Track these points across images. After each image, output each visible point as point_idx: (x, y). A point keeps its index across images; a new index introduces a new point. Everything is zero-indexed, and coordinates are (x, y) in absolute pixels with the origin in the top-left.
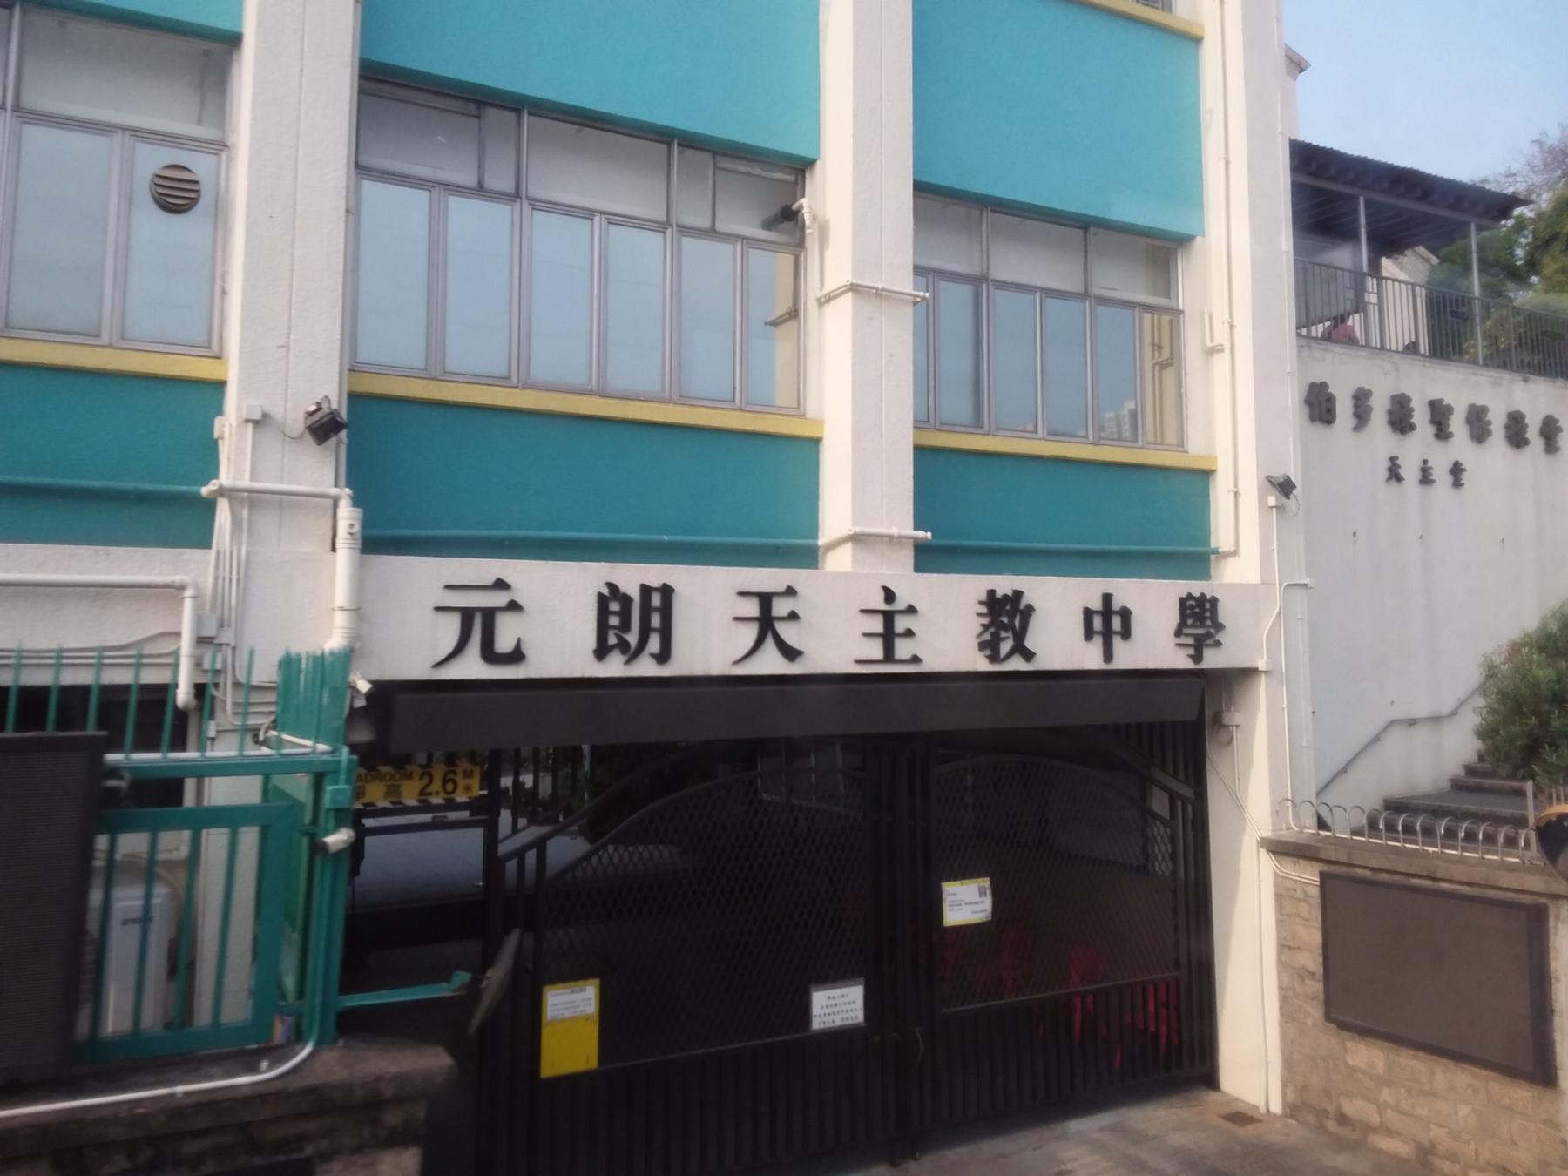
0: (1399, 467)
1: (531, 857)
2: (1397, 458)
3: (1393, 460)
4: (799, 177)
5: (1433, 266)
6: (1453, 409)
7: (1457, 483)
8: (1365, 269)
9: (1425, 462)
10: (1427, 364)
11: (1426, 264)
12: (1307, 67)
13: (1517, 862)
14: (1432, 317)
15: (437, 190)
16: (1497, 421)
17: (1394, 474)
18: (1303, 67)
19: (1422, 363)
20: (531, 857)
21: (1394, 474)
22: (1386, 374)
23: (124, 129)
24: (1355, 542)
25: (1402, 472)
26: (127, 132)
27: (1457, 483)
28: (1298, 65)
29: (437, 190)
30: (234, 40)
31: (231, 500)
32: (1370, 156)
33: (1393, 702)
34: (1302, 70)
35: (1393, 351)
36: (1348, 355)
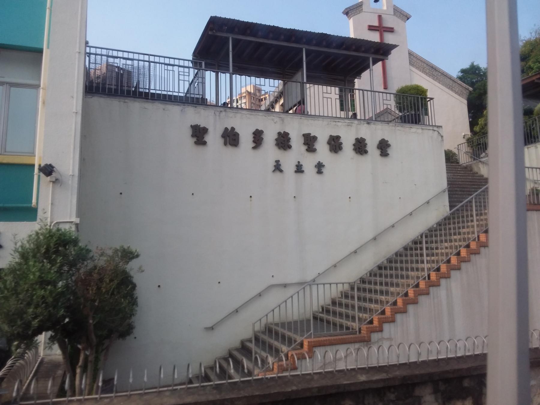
0: (280, 165)
1: (277, 311)
2: (279, 161)
3: (277, 162)
4: (87, 66)
5: (470, 92)
6: (207, 129)
7: (320, 172)
8: (305, 81)
9: (299, 162)
10: (303, 118)
11: (467, 90)
12: (410, 17)
13: (319, 358)
14: (426, 108)
15: (5, 85)
16: (348, 142)
17: (278, 167)
18: (409, 17)
19: (299, 117)
20: (277, 311)
21: (278, 167)
22: (275, 123)
23: (7, 83)
24: (251, 201)
25: (282, 168)
26: (8, 84)
27: (320, 172)
28: (406, 16)
29: (5, 85)
30: (40, 52)
31: (531, 204)
32: (297, 28)
33: (273, 276)
34: (408, 19)
35: (363, 120)
36: (251, 115)
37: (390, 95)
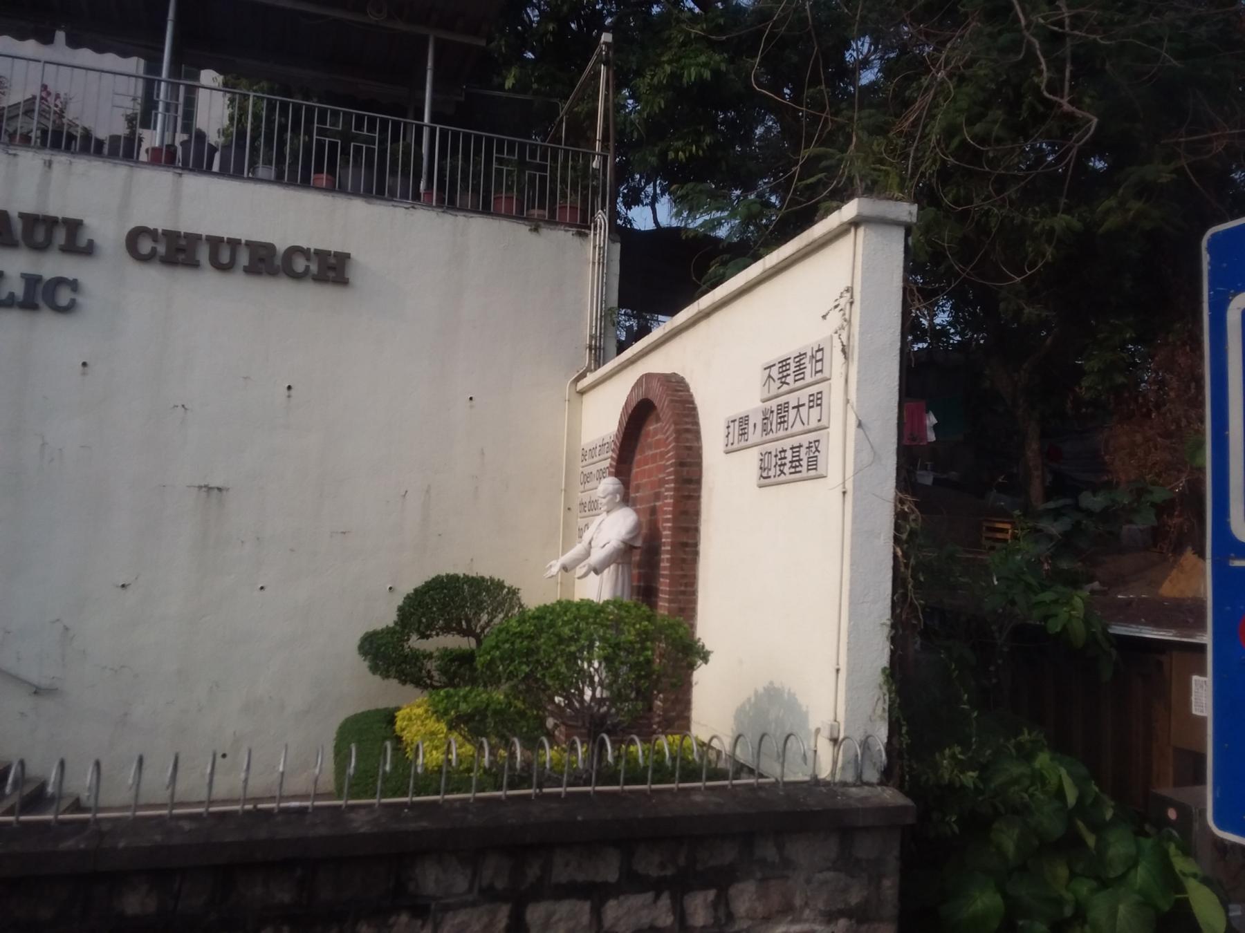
37: (211, 94)
